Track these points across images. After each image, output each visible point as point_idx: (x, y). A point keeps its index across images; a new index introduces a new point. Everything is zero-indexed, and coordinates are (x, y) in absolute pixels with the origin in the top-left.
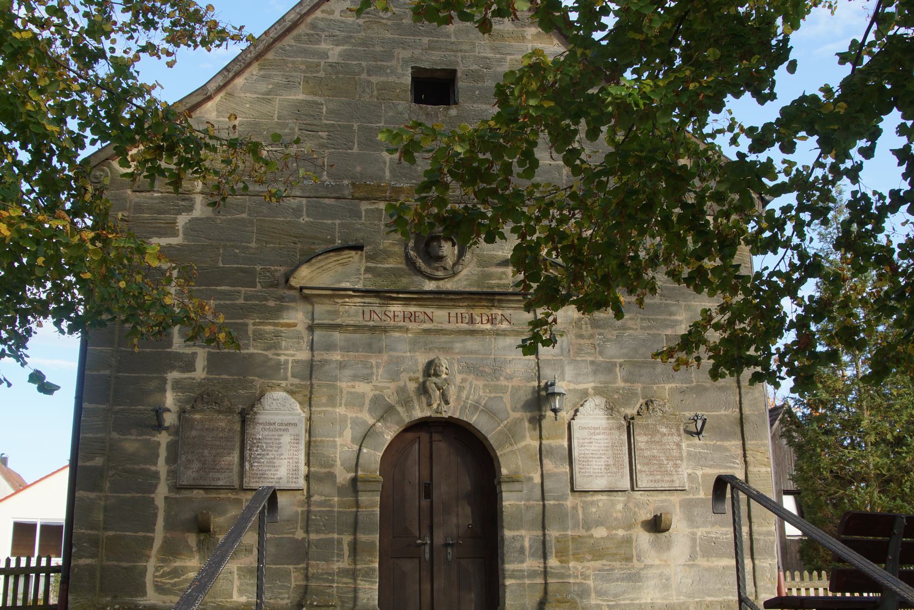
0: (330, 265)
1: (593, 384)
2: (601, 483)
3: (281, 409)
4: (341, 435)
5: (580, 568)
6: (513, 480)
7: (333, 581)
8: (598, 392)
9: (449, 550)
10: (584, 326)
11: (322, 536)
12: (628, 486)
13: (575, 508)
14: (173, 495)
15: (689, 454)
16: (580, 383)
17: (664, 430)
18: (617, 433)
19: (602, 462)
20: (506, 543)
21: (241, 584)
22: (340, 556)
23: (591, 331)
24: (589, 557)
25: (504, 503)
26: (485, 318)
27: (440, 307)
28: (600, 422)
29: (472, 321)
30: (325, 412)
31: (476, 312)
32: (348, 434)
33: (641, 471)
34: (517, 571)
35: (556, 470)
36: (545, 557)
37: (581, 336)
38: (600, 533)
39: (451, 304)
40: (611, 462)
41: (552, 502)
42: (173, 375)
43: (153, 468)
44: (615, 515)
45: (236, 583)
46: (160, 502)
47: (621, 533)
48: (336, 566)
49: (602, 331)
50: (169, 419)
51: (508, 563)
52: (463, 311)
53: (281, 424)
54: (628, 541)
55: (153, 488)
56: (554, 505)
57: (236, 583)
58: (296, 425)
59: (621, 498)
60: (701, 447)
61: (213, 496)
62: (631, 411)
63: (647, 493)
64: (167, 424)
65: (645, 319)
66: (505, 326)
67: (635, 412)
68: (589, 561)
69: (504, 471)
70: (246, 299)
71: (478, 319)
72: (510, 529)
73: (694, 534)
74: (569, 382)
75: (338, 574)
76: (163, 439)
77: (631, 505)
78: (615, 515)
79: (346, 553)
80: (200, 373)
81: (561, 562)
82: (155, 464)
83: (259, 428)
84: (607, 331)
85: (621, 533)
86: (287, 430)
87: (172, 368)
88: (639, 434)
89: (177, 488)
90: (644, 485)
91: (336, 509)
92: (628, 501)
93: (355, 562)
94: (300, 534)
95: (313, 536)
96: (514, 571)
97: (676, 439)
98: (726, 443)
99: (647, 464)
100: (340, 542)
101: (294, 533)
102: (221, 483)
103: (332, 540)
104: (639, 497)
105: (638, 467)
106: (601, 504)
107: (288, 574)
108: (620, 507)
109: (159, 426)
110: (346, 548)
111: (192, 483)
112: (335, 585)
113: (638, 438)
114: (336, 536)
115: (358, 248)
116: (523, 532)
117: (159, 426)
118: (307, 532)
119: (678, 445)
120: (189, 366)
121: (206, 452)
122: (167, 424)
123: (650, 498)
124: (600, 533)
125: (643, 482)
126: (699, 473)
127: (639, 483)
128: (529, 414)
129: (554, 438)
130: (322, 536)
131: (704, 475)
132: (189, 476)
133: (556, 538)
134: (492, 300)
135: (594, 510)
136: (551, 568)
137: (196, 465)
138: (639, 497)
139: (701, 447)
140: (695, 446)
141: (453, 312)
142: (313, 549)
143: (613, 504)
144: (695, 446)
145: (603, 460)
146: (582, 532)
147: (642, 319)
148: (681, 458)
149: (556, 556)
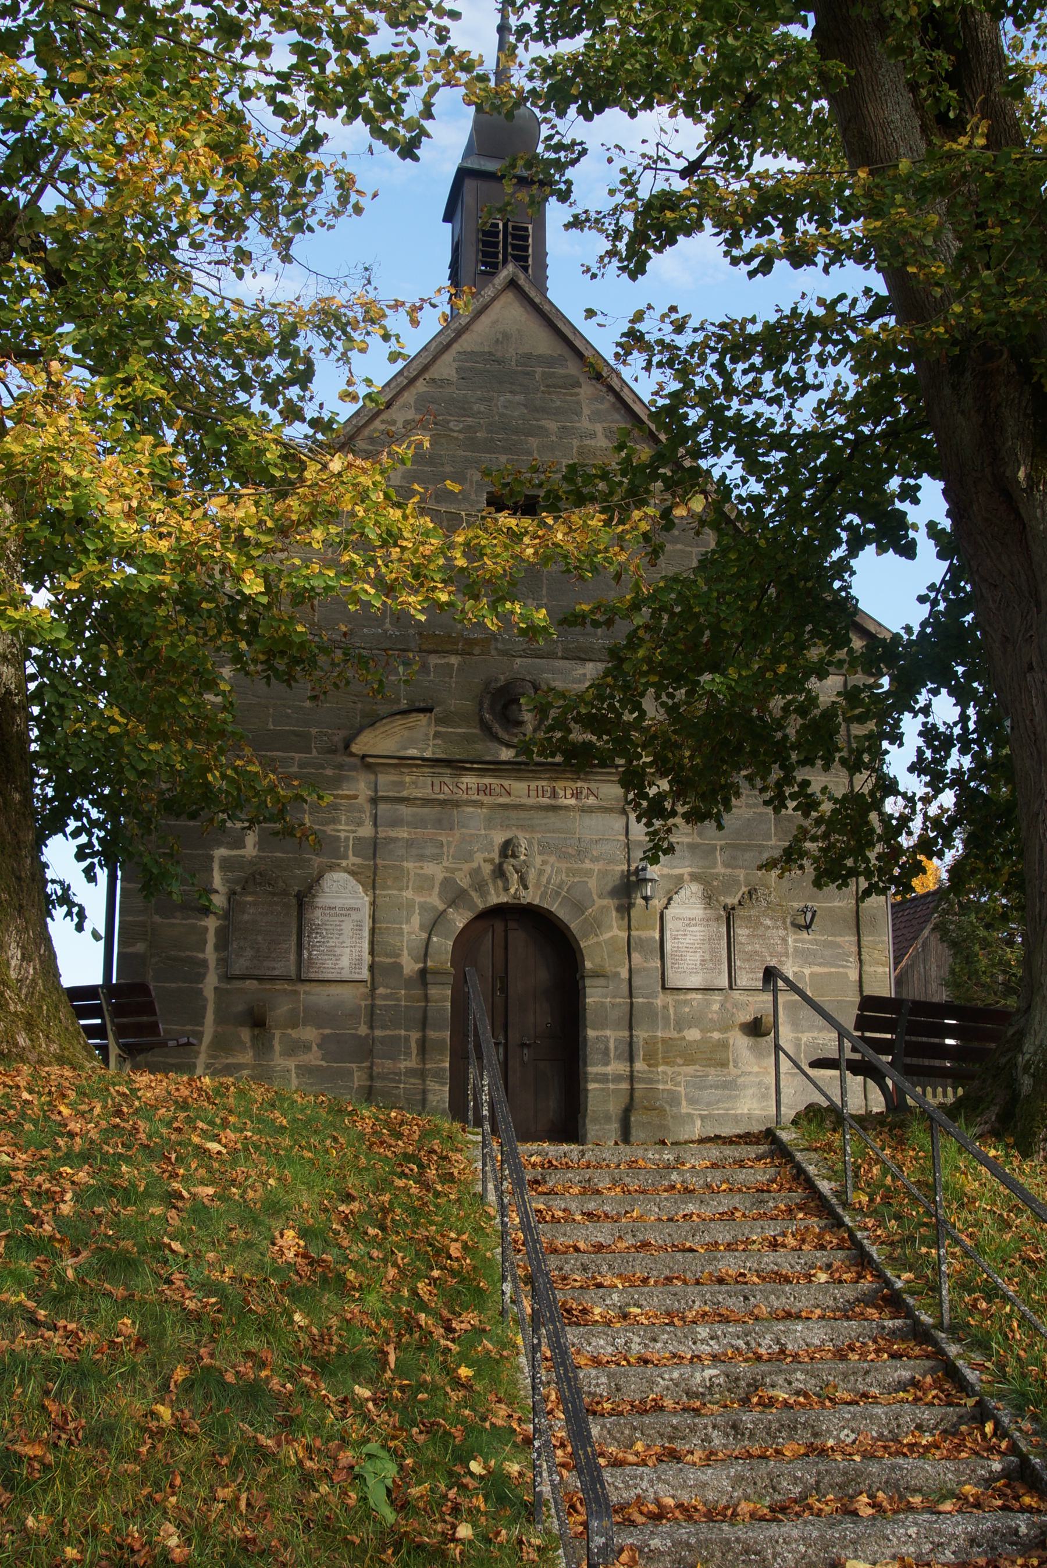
2: (695, 980)
3: (342, 894)
13: (665, 1007)
15: (796, 950)
17: (768, 922)
19: (697, 957)
24: (679, 1061)
38: (693, 1034)
47: (716, 1035)
51: (595, 1065)
54: (724, 1045)
59: (717, 997)
60: (811, 942)
66: (591, 801)
69: (588, 965)
70: (300, 766)
73: (799, 1039)
77: (728, 1005)
83: (318, 913)
85: (716, 1035)
97: (782, 932)
98: (839, 939)
100: (407, 1039)
108: (716, 1007)
116: (608, 1033)
119: (784, 940)
124: (693, 1034)
126: (807, 971)
131: (812, 974)
139: (811, 942)
140: (803, 941)
141: (533, 785)
143: (709, 1003)
144: (803, 941)
146: (675, 1035)
148: (787, 955)
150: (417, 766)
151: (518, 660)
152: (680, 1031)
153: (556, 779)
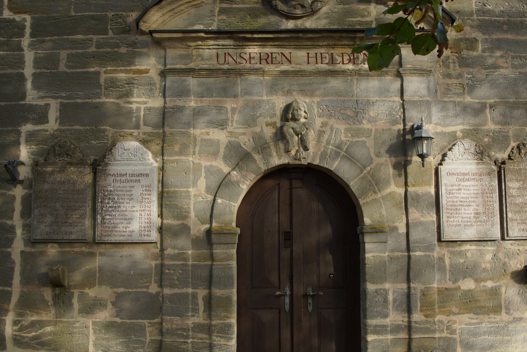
0: (183, 7)
1: (461, 127)
2: (470, 233)
4: (195, 184)
5: (446, 322)
6: (377, 230)
7: (187, 337)
8: (467, 134)
9: (310, 301)
10: (451, 65)
11: (176, 291)
12: (497, 233)
14: (28, 249)
16: (448, 125)
18: (486, 178)
19: (471, 210)
20: (369, 297)
21: (97, 339)
22: (195, 310)
23: (458, 70)
25: (367, 255)
26: (346, 58)
27: (299, 47)
28: (469, 167)
29: (332, 61)
30: (177, 161)
31: (337, 52)
32: (202, 183)
33: (512, 220)
34: (380, 326)
35: (422, 219)
36: (409, 311)
37: (448, 76)
40: (481, 209)
41: (418, 253)
42: (27, 128)
43: (9, 222)
44: (483, 266)
45: (92, 337)
46: (16, 257)
47: (490, 284)
48: (190, 322)
49: (471, 70)
50: (23, 172)
52: (323, 50)
53: (133, 175)
55: (9, 242)
56: (420, 256)
57: (92, 337)
58: (147, 175)
59: (490, 248)
61: (67, 249)
62: (502, 156)
63: (517, 242)
64: (21, 178)
65: (516, 57)
67: (505, 156)
68: (455, 314)
69: (367, 221)
70: (98, 47)
71: (339, 59)
72: (373, 283)
74: (437, 124)
75: (193, 329)
76: (19, 192)
77: (501, 255)
78: (483, 266)
79: (201, 307)
80: (52, 124)
81: (426, 316)
82: (11, 218)
83: (111, 179)
84: (476, 70)
86: (139, 181)
87: (26, 120)
88: (511, 180)
89: (31, 242)
90: (516, 234)
91: (190, 263)
92: (498, 251)
93: (210, 317)
94: (154, 289)
95: (167, 291)
96: (376, 326)
99: (519, 212)
100: (194, 296)
101: (148, 287)
102: (73, 237)
103: (186, 295)
104: (509, 246)
105: (510, 215)
106: (469, 255)
107: (143, 329)
108: (489, 257)
109: (14, 180)
110: (201, 302)
111: (45, 237)
112: (190, 341)
113: (509, 184)
114: (190, 290)
117: (14, 180)
118: (161, 286)
120: (43, 119)
121: (58, 205)
122: (21, 178)
123: (521, 248)
125: (514, 231)
127: (510, 232)
128: (393, 159)
129: (420, 185)
130: (176, 291)
132: (42, 230)
133: (422, 291)
135: (462, 261)
136: (416, 322)
137: (49, 219)
138: (509, 246)
141: (312, 52)
142: (167, 304)
143: (482, 254)
145: (472, 208)
147: (513, 57)
152: (455, 281)
153: (334, 46)
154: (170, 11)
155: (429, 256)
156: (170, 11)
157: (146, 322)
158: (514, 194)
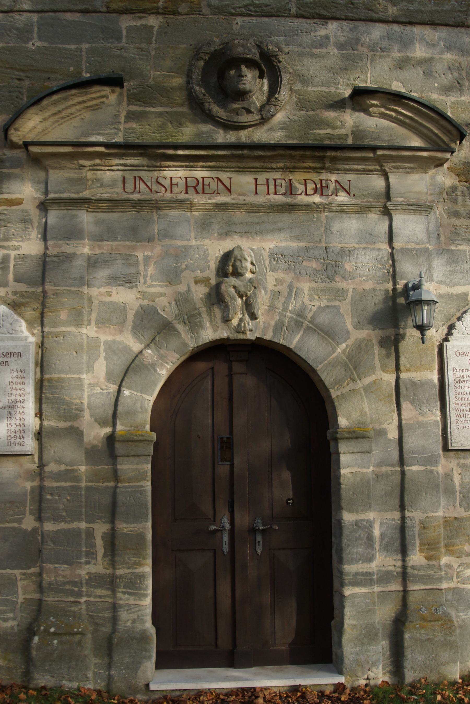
0: (73, 110)
16: (455, 285)
20: (346, 532)
25: (342, 471)
39: (258, 164)
74: (440, 283)
81: (428, 558)
100: (90, 534)
101: (20, 521)
115: (115, 82)
134: (322, 159)
149: (421, 551)
150: (100, 155)
151: (239, 20)
154: (54, 114)
155: (431, 471)
156: (54, 114)
157: (17, 572)
158: (358, 414)
